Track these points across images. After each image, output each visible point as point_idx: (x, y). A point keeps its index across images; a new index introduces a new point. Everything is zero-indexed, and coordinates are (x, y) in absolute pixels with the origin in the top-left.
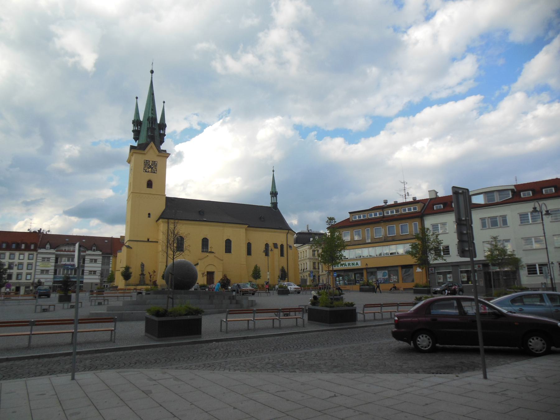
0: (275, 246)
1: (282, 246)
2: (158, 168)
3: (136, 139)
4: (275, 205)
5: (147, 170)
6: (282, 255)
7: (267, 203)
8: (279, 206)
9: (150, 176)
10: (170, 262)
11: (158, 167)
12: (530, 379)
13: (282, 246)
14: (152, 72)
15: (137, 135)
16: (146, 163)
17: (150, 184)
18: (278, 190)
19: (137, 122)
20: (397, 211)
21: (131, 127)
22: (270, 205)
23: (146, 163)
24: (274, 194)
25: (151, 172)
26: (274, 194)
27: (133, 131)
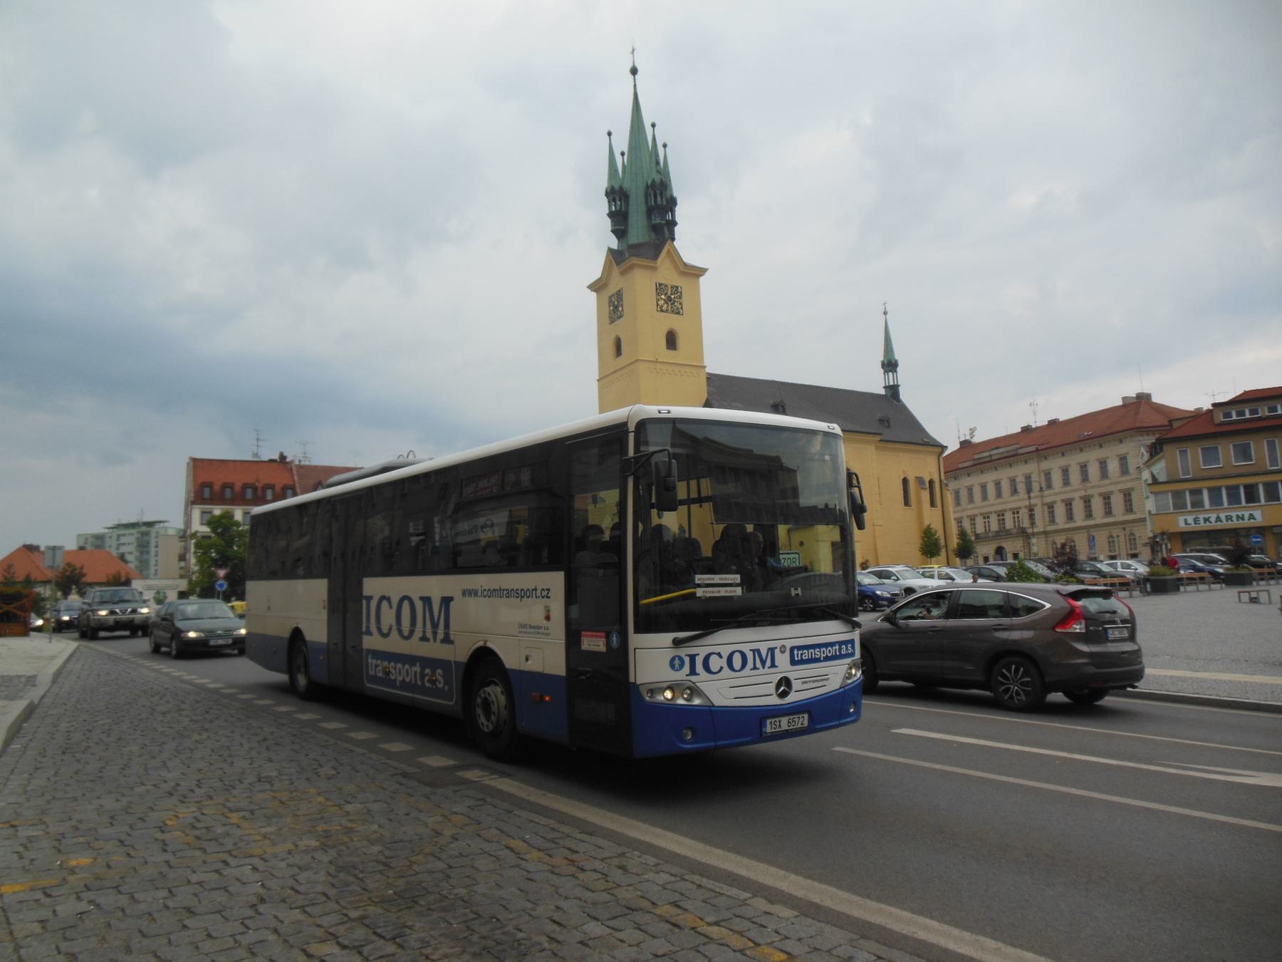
0: (920, 480)
1: (931, 482)
2: (685, 300)
3: (620, 233)
4: (893, 391)
5: (665, 307)
6: (933, 504)
7: (874, 383)
8: (904, 396)
9: (669, 321)
10: (1043, 570)
11: (686, 300)
12: (722, 586)
13: (931, 482)
14: (634, 71)
15: (620, 220)
16: (660, 288)
17: (671, 341)
18: (898, 355)
19: (616, 195)
20: (1253, 412)
21: (603, 206)
22: (883, 392)
23: (660, 288)
24: (890, 365)
25: (673, 312)
26: (890, 365)
27: (611, 215)
